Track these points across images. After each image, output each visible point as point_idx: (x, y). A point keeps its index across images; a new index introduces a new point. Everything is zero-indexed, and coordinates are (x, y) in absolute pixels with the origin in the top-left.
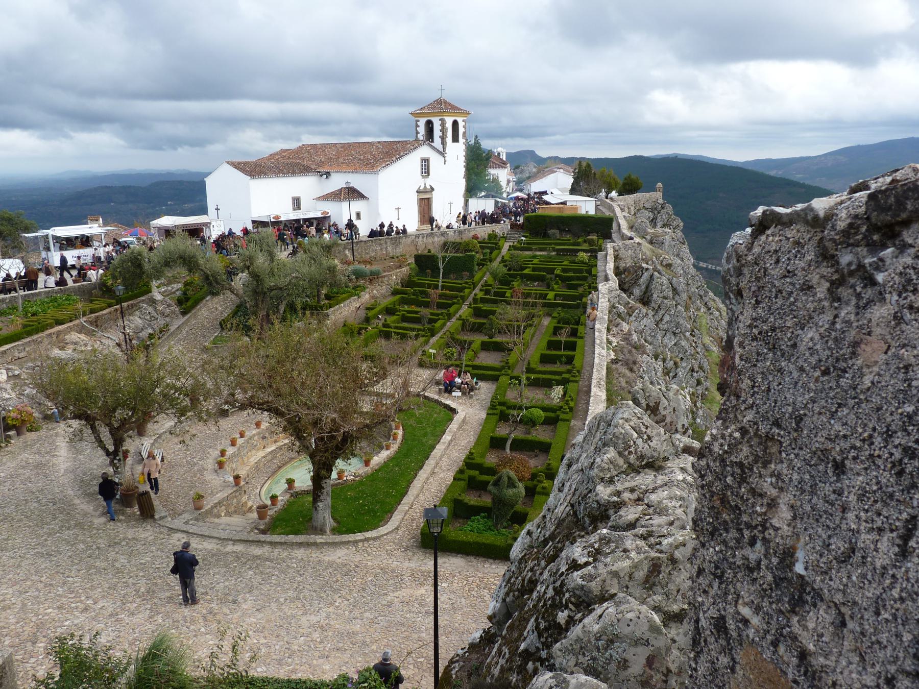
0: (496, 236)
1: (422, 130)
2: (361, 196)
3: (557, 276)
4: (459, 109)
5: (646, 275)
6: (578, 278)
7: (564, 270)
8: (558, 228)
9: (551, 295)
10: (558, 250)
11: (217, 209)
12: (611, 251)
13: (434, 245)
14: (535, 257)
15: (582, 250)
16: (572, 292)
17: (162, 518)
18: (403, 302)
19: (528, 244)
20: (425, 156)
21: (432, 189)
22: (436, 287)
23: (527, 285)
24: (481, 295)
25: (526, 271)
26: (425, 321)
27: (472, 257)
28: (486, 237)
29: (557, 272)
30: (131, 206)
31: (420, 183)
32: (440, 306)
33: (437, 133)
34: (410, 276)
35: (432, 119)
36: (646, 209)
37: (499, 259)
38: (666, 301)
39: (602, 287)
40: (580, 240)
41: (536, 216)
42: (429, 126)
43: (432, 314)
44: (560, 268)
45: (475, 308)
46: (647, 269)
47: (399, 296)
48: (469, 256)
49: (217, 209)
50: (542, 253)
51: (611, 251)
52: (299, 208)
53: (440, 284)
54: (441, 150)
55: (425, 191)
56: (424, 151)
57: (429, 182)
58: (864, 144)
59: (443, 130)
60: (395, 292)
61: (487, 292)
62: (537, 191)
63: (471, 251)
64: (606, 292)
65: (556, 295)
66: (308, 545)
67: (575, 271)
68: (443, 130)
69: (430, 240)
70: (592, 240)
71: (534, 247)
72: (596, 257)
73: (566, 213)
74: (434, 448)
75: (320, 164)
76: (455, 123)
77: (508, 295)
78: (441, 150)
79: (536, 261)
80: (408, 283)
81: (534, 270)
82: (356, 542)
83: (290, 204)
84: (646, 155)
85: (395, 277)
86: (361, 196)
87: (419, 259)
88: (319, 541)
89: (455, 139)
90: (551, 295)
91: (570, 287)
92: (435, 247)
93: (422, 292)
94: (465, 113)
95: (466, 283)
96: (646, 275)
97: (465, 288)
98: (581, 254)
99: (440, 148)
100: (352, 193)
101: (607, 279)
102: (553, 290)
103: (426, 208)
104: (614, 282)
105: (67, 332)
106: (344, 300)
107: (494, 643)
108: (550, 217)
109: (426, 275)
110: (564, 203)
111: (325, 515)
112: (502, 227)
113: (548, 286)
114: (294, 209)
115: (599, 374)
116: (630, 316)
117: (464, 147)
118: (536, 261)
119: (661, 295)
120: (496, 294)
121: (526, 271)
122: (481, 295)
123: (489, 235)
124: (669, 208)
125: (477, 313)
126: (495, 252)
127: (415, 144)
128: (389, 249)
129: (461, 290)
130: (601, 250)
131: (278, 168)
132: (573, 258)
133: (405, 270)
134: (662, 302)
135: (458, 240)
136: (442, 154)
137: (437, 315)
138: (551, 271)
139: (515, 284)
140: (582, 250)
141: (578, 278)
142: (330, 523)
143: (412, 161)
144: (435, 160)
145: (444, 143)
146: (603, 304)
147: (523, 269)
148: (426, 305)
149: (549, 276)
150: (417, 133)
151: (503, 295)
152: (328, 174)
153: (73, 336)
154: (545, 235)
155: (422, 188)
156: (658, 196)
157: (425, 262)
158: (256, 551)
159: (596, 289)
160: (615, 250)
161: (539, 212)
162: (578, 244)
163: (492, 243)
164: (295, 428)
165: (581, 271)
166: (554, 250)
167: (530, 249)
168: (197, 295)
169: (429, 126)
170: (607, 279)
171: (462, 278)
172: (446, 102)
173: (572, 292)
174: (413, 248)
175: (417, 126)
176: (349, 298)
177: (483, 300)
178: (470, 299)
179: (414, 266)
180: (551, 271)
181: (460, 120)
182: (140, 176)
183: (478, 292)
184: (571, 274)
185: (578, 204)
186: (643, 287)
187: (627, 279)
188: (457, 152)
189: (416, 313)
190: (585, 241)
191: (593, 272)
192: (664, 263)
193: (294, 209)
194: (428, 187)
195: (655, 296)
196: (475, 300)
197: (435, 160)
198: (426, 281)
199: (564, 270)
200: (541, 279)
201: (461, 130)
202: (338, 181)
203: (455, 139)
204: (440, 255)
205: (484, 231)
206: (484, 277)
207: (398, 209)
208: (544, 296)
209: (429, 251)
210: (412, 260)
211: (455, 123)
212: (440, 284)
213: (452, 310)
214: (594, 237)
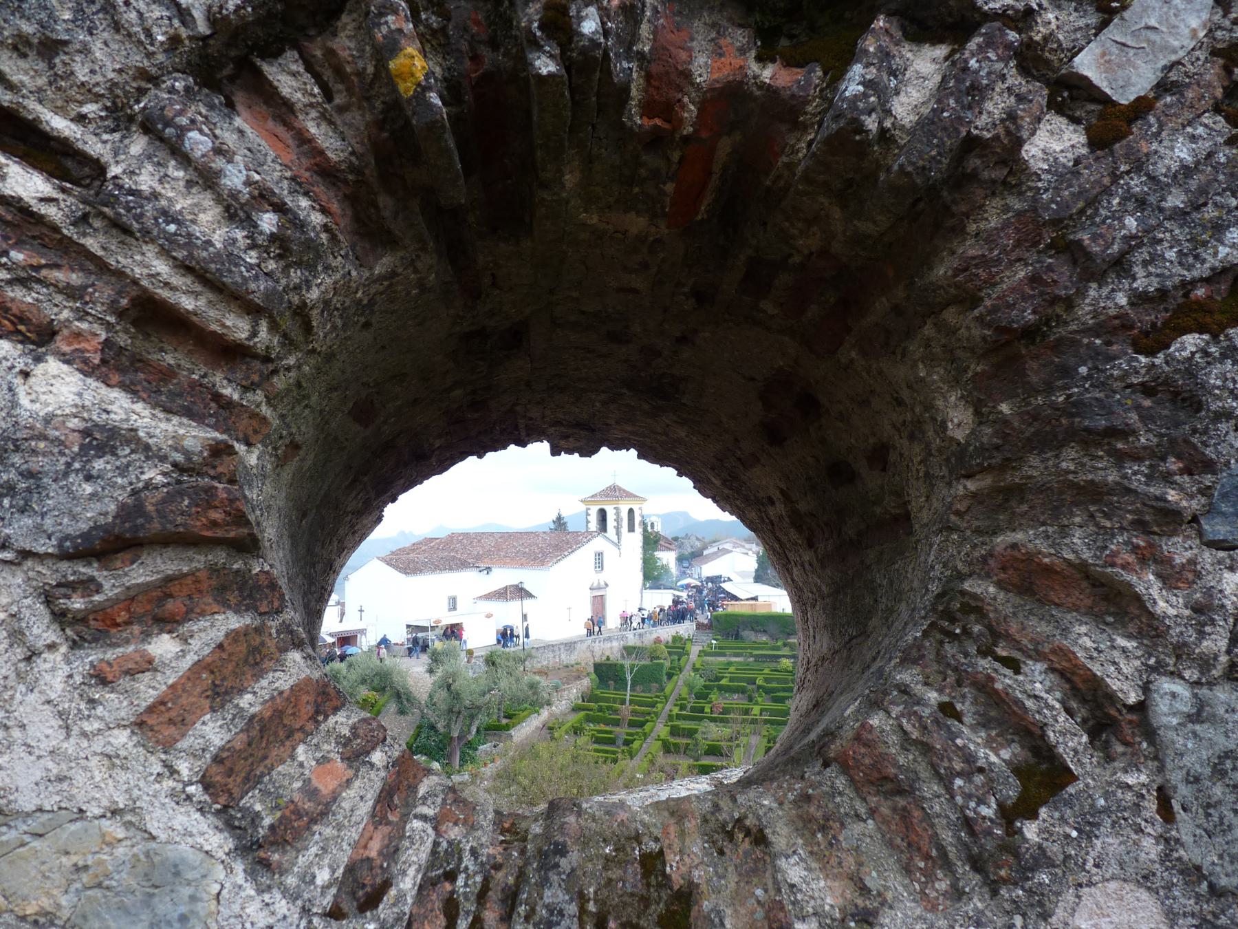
0: (681, 639)
3: (759, 687)
4: (635, 496)
6: (785, 690)
7: (766, 680)
8: (753, 629)
9: (756, 710)
10: (756, 656)
11: (361, 611)
13: (610, 649)
14: (730, 664)
15: (784, 656)
16: (778, 706)
18: (589, 719)
19: (720, 648)
20: (599, 549)
22: (623, 702)
23: (726, 698)
24: (676, 711)
25: (723, 682)
26: (620, 742)
27: (661, 665)
28: (670, 639)
29: (760, 682)
31: (596, 578)
32: (632, 724)
33: (611, 523)
35: (607, 508)
37: (689, 667)
40: (780, 643)
41: (727, 615)
42: (603, 515)
43: (628, 734)
44: (761, 677)
45: (672, 727)
47: (583, 713)
48: (658, 664)
49: (361, 611)
50: (737, 659)
53: (628, 698)
56: (599, 543)
57: (602, 577)
60: (576, 709)
61: (682, 708)
62: (710, 575)
63: (658, 658)
65: (762, 710)
67: (778, 681)
68: (618, 520)
69: (608, 645)
71: (728, 652)
73: (761, 611)
74: (1051, 749)
75: (478, 557)
76: (631, 511)
77: (707, 710)
79: (732, 669)
80: (589, 697)
81: (731, 680)
83: (445, 604)
85: (574, 692)
87: (598, 667)
89: (631, 529)
90: (756, 710)
91: (777, 700)
93: (609, 708)
94: (643, 500)
95: (658, 697)
98: (784, 661)
99: (615, 539)
100: (520, 592)
102: (757, 703)
106: (525, 717)
108: (742, 616)
109: (608, 687)
110: (755, 599)
112: (686, 629)
113: (750, 699)
114: (450, 610)
117: (640, 538)
118: (732, 669)
120: (693, 709)
121: (723, 682)
122: (676, 711)
123: (674, 638)
125: (675, 732)
126: (684, 658)
128: (563, 656)
129: (653, 705)
131: (433, 563)
132: (774, 665)
133: (586, 682)
135: (639, 644)
137: (631, 735)
138: (752, 681)
140: (784, 656)
141: (785, 690)
144: (610, 552)
147: (718, 679)
148: (617, 723)
149: (750, 687)
151: (702, 710)
152: (488, 569)
154: (737, 636)
157: (606, 672)
161: (730, 610)
162: (778, 649)
163: (678, 647)
165: (785, 681)
167: (724, 655)
169: (603, 515)
172: (620, 489)
173: (778, 706)
174: (589, 654)
175: (588, 514)
176: (528, 716)
177: (679, 717)
178: (664, 715)
179: (594, 676)
180: (752, 681)
181: (636, 508)
183: (671, 708)
184: (774, 685)
185: (772, 599)
188: (633, 542)
189: (610, 732)
190: (785, 645)
193: (450, 610)
194: (602, 584)
196: (670, 717)
197: (610, 552)
198: (611, 693)
200: (742, 691)
201: (637, 519)
203: (631, 529)
204: (627, 663)
205: (667, 632)
206: (679, 686)
208: (747, 712)
209: (608, 658)
210: (592, 670)
211: (631, 511)
212: (628, 698)
213: (647, 727)
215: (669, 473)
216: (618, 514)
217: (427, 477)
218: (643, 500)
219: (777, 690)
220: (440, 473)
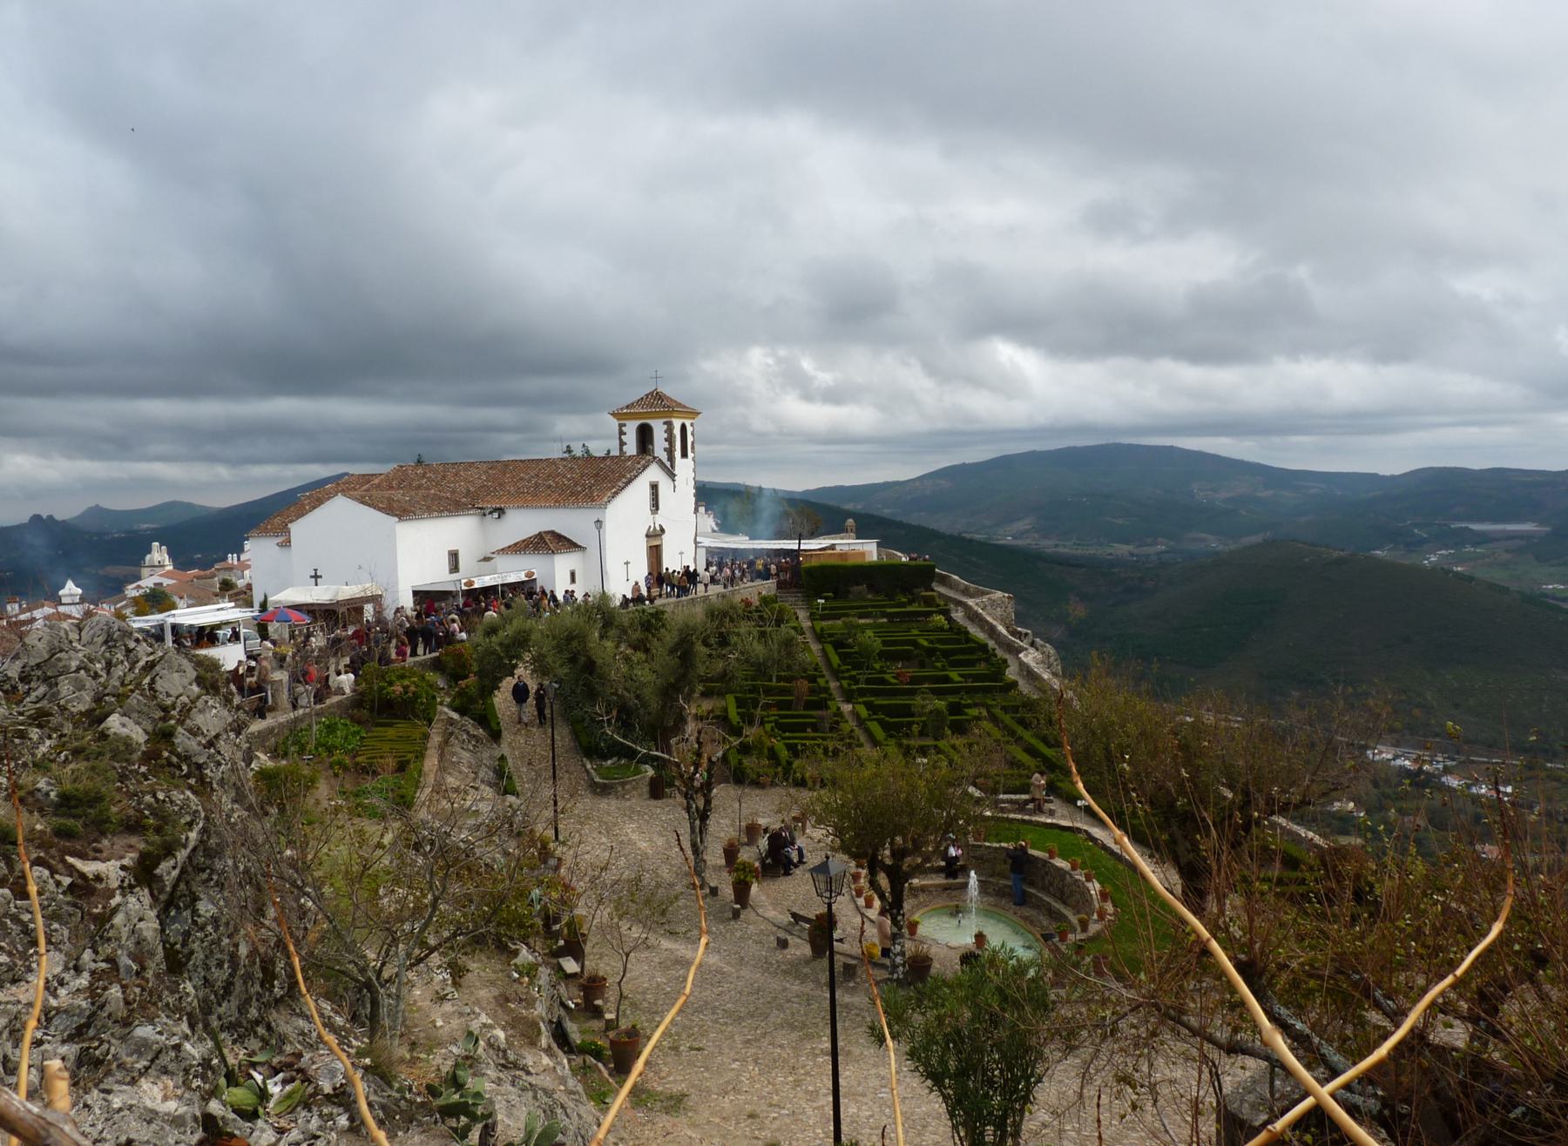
10: (890, 616)
20: (654, 479)
21: (663, 530)
35: (653, 423)
42: (645, 435)
56: (653, 473)
57: (660, 519)
58: (1211, 451)
59: (670, 439)
68: (670, 439)
76: (683, 428)
89: (684, 455)
94: (694, 414)
107: (263, 717)
115: (1295, 827)
136: (671, 475)
145: (671, 458)
150: (622, 444)
152: (501, 511)
164: (81, 620)
166: (884, 615)
169: (645, 435)
175: (622, 433)
181: (688, 423)
201: (690, 439)
202: (524, 522)
203: (684, 455)
211: (683, 428)
215: (1388, 473)
216: (670, 430)
217: (1393, 477)
218: (694, 414)
219: (954, 652)
220: (1375, 475)
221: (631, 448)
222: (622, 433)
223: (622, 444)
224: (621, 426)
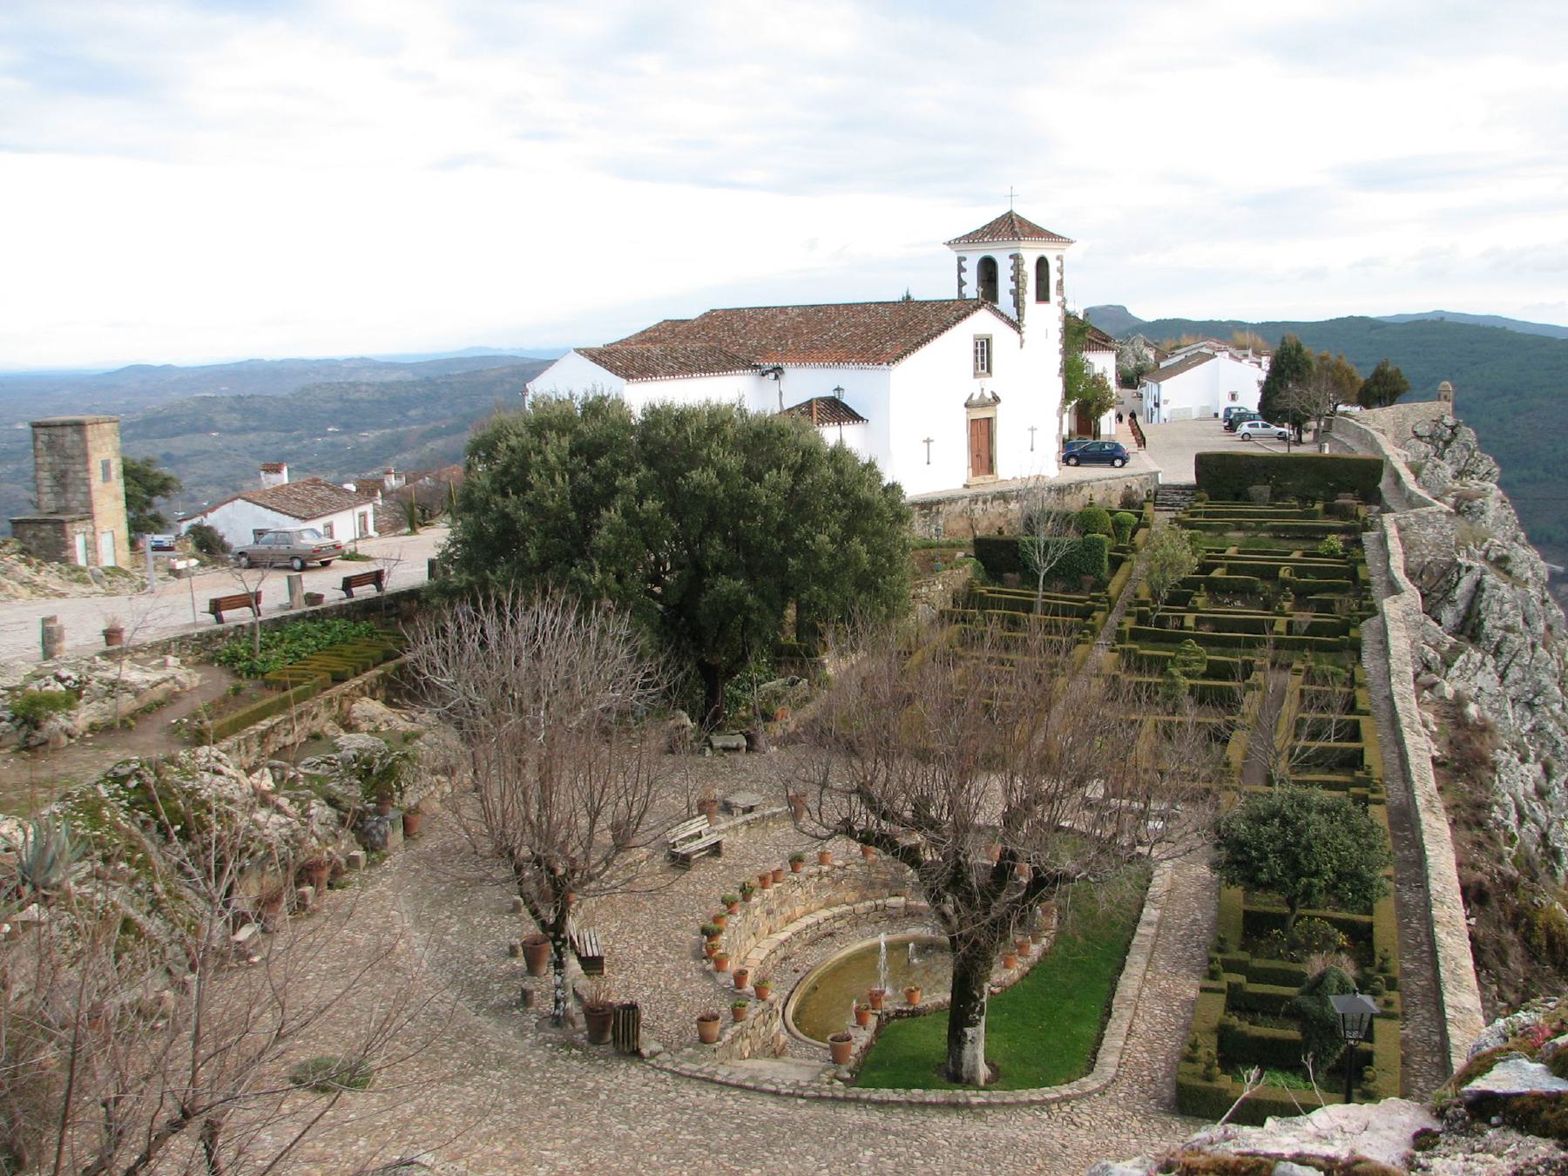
1: (972, 277)
2: (854, 417)
5: (1466, 583)
10: (1272, 529)
12: (1392, 531)
17: (653, 1055)
21: (996, 399)
30: (252, 436)
34: (969, 584)
36: (1419, 437)
38: (1511, 636)
39: (1391, 608)
42: (988, 270)
46: (1469, 569)
51: (1392, 531)
52: (990, 467)
54: (1015, 318)
55: (984, 404)
56: (982, 322)
57: (989, 385)
59: (1017, 278)
64: (1401, 621)
66: (955, 1106)
68: (1017, 278)
70: (1344, 506)
72: (1358, 543)
76: (1042, 264)
78: (1015, 318)
81: (1231, 569)
82: (1045, 1104)
84: (1373, 313)
86: (854, 417)
88: (974, 1100)
89: (1043, 295)
92: (1009, 523)
96: (1466, 583)
97: (1093, 609)
101: (1394, 589)
103: (984, 438)
104: (1411, 595)
105: (350, 697)
111: (977, 1053)
115: (1425, 784)
116: (1449, 666)
119: (1499, 624)
121: (1217, 573)
122: (1129, 623)
124: (1468, 435)
127: (956, 311)
130: (1366, 528)
134: (1504, 639)
136: (1016, 326)
138: (1270, 574)
139: (1200, 601)
142: (983, 1071)
143: (956, 342)
145: (1018, 303)
146: (1399, 642)
152: (778, 371)
153: (366, 706)
155: (976, 398)
156: (1442, 409)
158: (851, 1116)
159: (1373, 611)
160: (1401, 529)
168: (310, 626)
169: (988, 270)
170: (1394, 589)
171: (1079, 590)
182: (277, 371)
184: (1312, 580)
186: (1461, 606)
187: (1436, 585)
188: (1044, 322)
191: (1362, 576)
192: (1492, 555)
195: (1487, 624)
199: (1299, 572)
201: (1054, 277)
203: (1043, 295)
207: (928, 441)
209: (1000, 532)
211: (1042, 264)
214: (1345, 500)
221: (972, 290)
222: (961, 269)
223: (961, 283)
224: (961, 260)
